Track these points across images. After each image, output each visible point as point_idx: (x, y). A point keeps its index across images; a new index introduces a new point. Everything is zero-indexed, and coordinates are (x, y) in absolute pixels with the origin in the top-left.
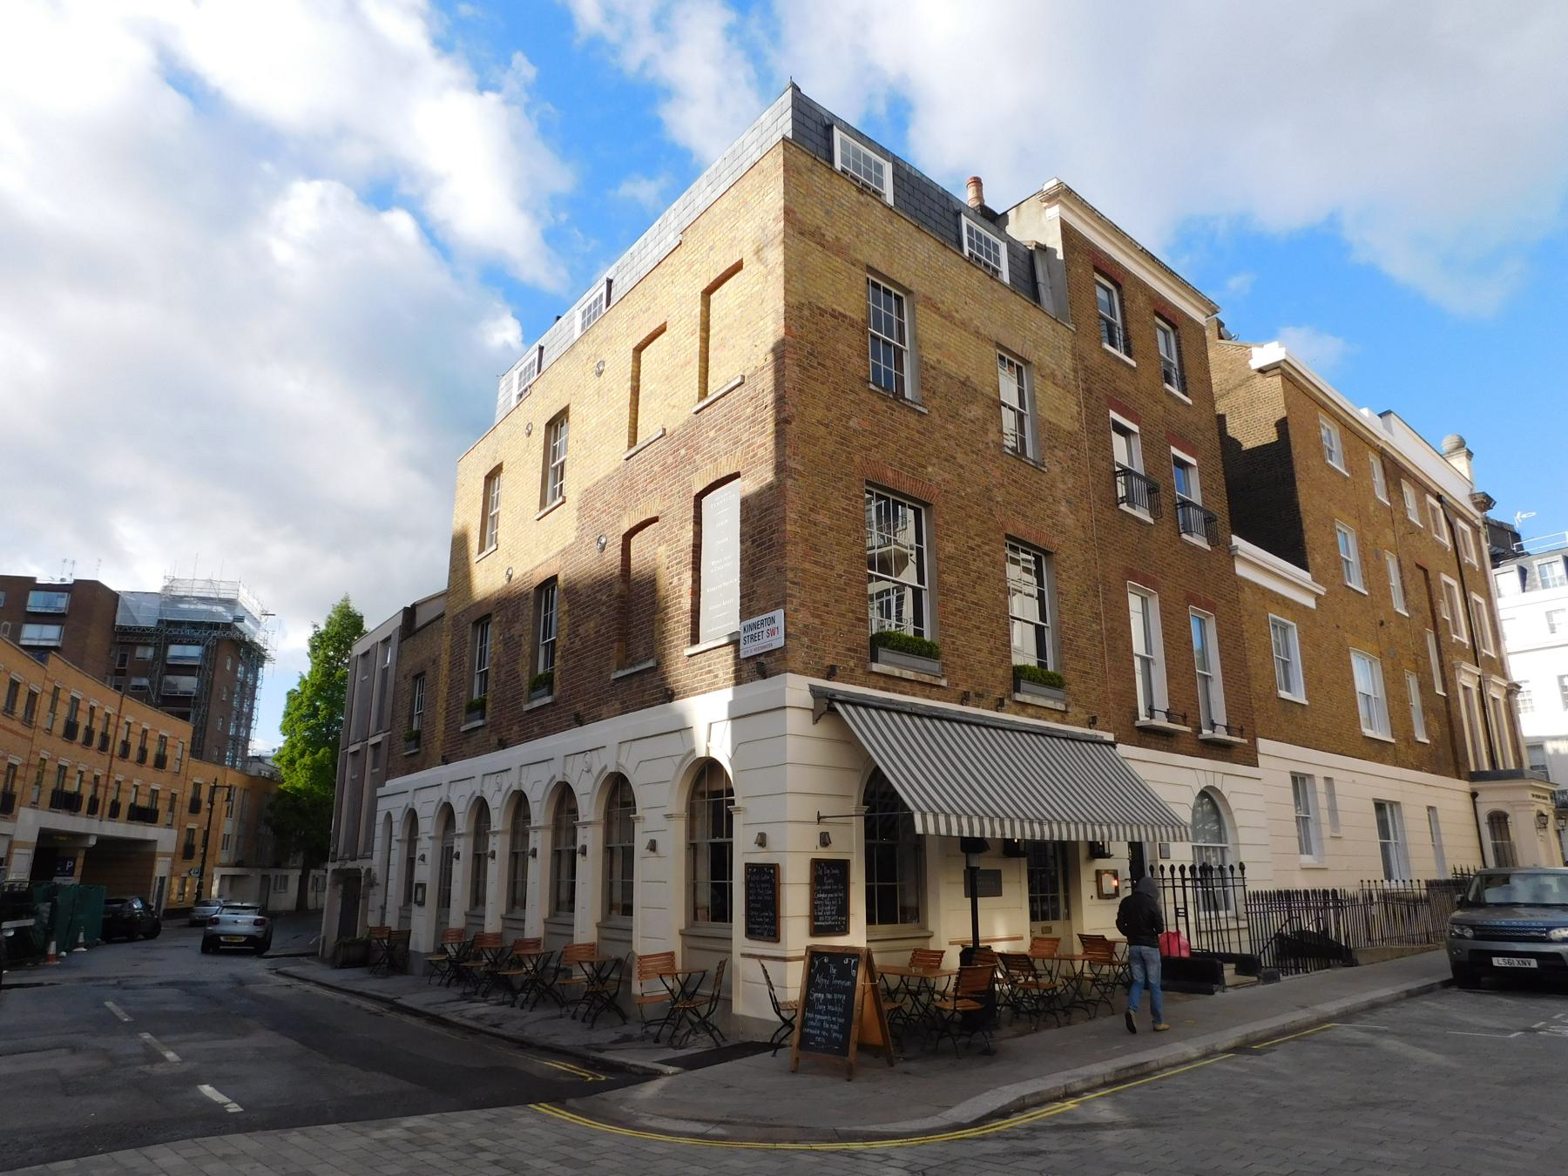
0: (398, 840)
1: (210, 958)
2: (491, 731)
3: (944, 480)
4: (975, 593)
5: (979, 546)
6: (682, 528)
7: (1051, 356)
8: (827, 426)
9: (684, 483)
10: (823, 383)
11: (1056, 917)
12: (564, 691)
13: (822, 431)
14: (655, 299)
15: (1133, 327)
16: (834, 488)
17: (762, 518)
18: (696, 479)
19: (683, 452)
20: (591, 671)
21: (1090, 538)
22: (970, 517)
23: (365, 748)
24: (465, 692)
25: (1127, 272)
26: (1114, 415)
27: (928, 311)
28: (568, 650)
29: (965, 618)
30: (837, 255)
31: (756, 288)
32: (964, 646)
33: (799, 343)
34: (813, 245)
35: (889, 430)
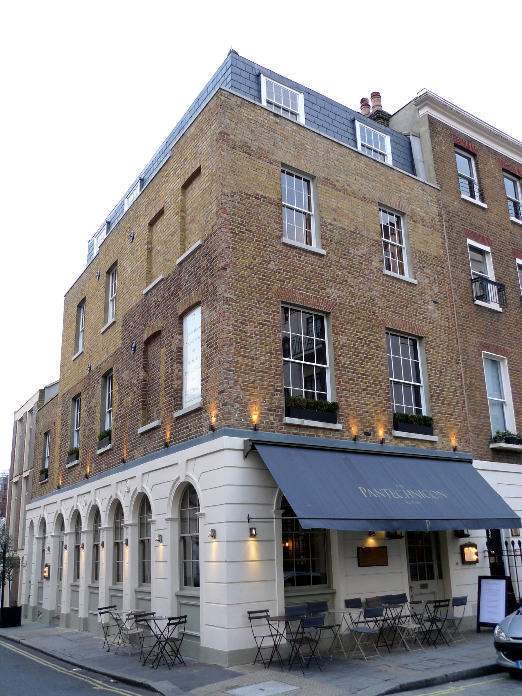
0: (36, 538)
1: (348, 609)
2: (81, 467)
3: (339, 297)
4: (363, 368)
5: (366, 337)
6: (173, 337)
7: (421, 208)
8: (252, 269)
9: (174, 309)
10: (250, 242)
11: (431, 577)
12: (117, 441)
13: (248, 272)
14: (158, 192)
15: (486, 182)
16: (258, 308)
17: (212, 330)
18: (179, 306)
19: (173, 289)
20: (129, 428)
21: (452, 325)
22: (359, 319)
23: (21, 479)
24: (69, 443)
25: (481, 145)
26: (470, 242)
27: (326, 187)
28: (119, 414)
29: (356, 384)
30: (259, 158)
31: (208, 184)
32: (355, 402)
33: (232, 218)
34: (242, 154)
35: (298, 267)
